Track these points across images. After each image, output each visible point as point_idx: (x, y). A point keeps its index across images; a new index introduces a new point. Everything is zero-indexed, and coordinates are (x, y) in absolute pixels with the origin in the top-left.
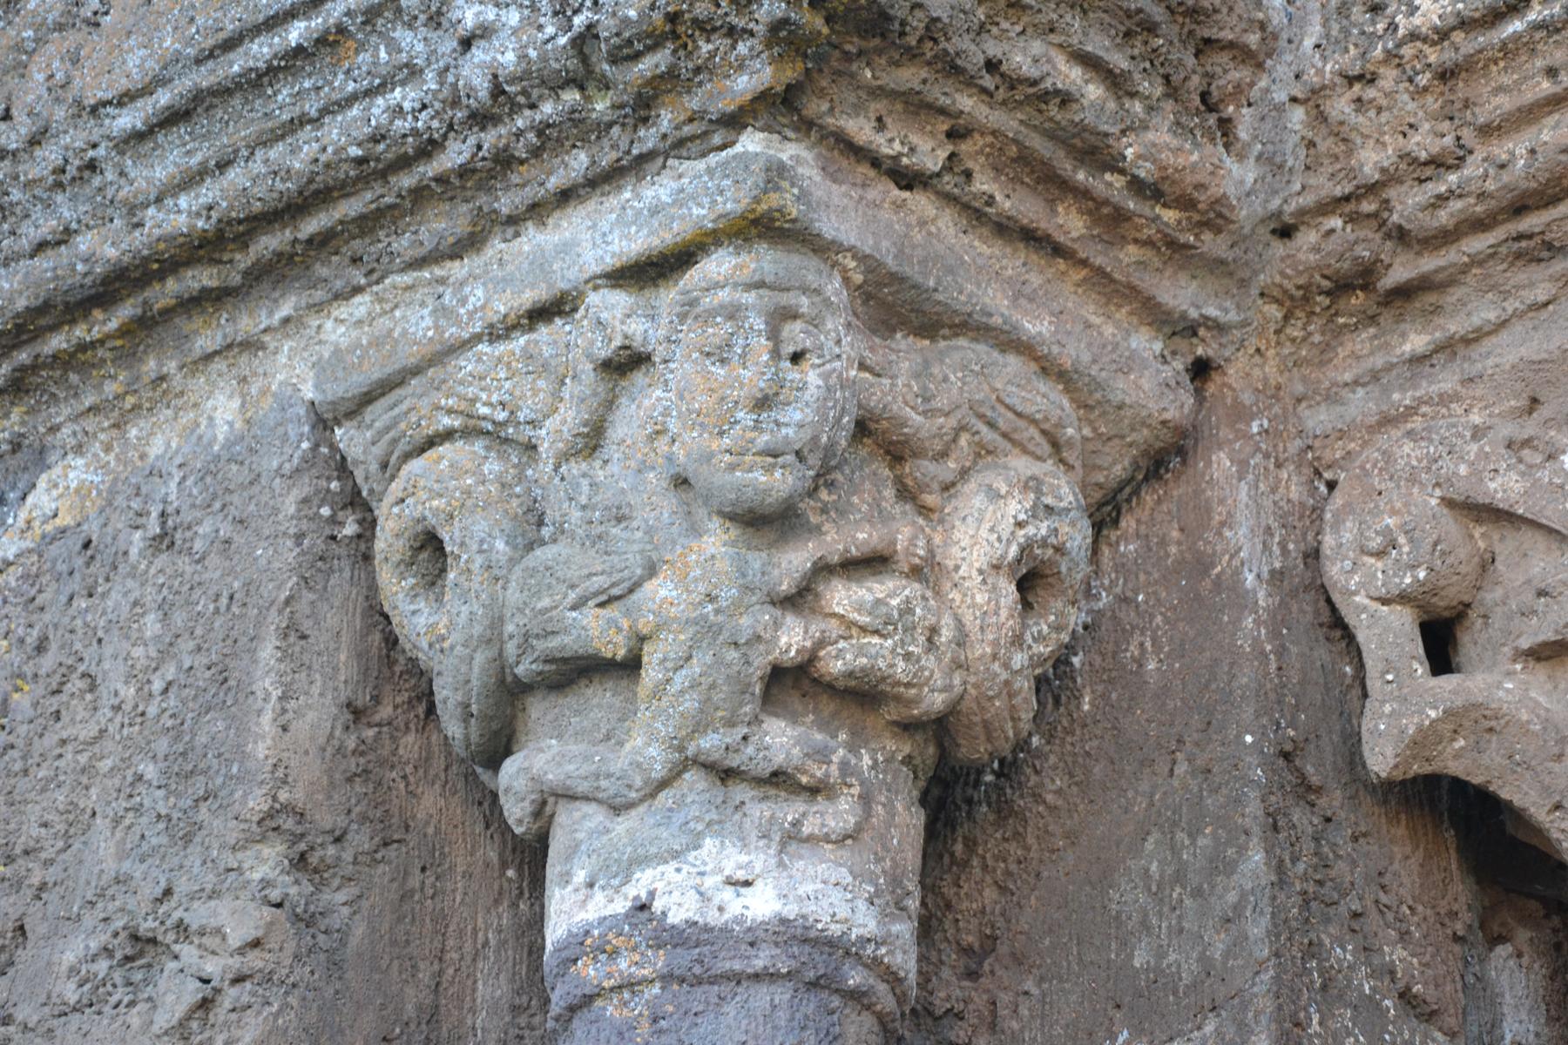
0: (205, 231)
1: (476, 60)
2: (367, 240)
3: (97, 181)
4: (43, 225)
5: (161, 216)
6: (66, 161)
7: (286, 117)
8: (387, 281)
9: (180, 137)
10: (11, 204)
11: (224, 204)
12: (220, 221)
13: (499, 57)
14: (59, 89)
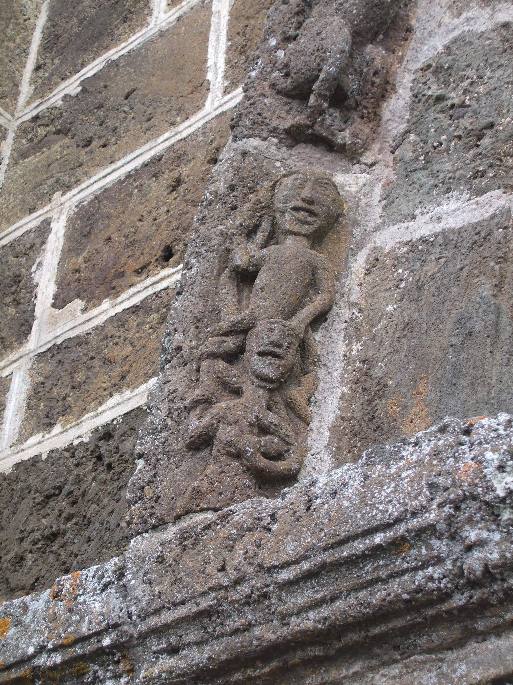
0: (321, 629)
1: (475, 556)
2: (403, 638)
3: (267, 602)
4: (240, 622)
5: (299, 620)
6: (252, 592)
7: (369, 578)
8: (412, 658)
9: (312, 584)
10: (223, 610)
11: (333, 617)
12: (330, 625)
13: (489, 556)
14: (248, 559)
